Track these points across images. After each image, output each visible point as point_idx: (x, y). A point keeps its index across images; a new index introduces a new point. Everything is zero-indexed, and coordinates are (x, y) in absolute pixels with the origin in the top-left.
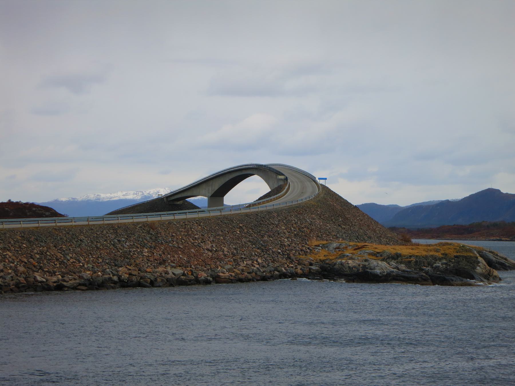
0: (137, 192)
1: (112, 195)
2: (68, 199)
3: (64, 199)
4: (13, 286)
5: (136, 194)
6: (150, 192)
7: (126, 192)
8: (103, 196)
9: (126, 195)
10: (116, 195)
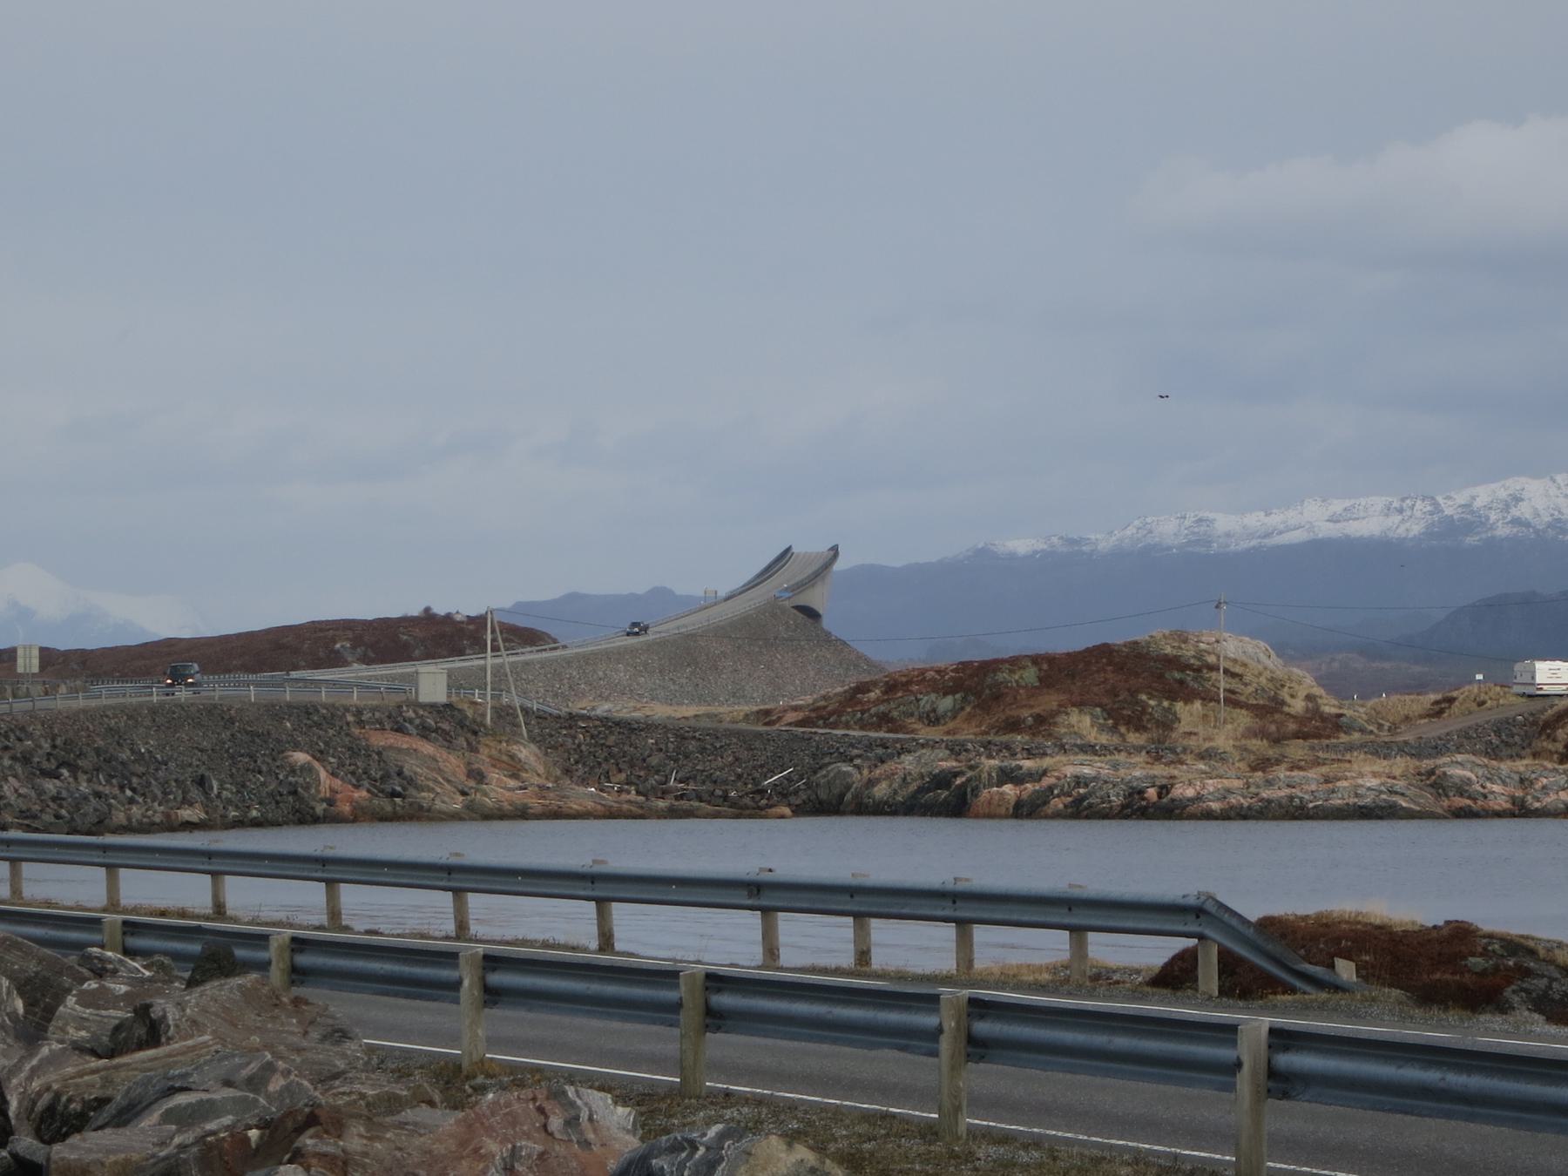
0: (1403, 500)
1: (1276, 520)
2: (1042, 546)
3: (1021, 545)
4: (101, 776)
5: (1401, 511)
6: (1473, 498)
7: (1347, 503)
8: (1224, 523)
9: (1348, 515)
10: (1292, 516)
